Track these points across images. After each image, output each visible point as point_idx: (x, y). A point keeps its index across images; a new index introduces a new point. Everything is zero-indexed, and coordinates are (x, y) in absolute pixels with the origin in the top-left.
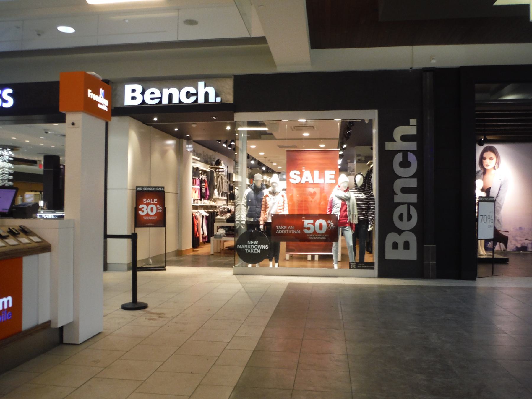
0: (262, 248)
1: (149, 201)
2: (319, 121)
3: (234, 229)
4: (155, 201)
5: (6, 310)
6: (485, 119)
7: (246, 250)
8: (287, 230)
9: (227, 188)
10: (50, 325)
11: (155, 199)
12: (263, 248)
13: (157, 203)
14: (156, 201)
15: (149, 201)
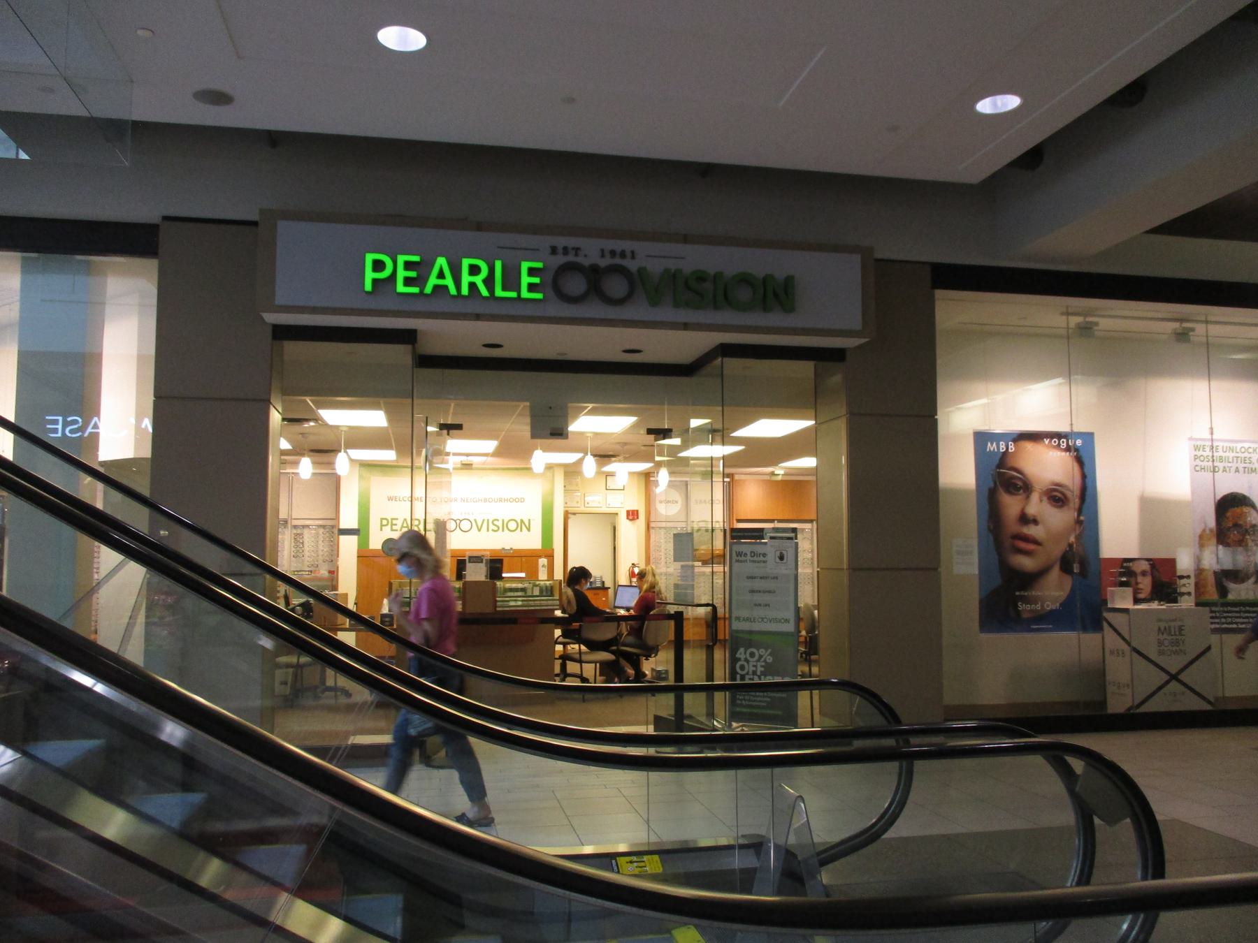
1: (441, 275)
2: (813, 578)
3: (96, 431)
4: (526, 280)
8: (60, 427)
13: (539, 296)
14: (536, 280)
15: (441, 275)
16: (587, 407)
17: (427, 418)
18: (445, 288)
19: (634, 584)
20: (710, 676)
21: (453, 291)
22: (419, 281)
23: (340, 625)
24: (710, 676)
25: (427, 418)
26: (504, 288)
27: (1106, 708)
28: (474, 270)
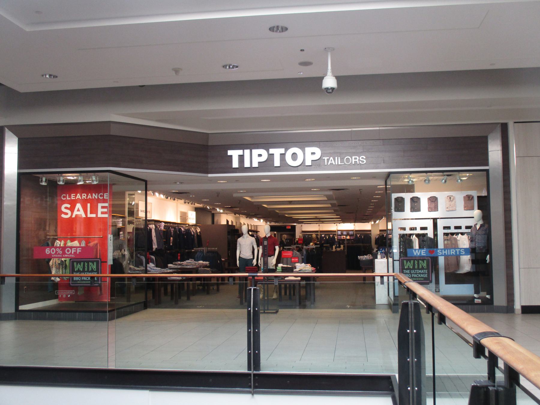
0: (97, 194)
1: (331, 161)
5: (375, 250)
6: (378, 128)
7: (193, 229)
9: (379, 273)
10: (426, 235)
11: (72, 195)
12: (96, 195)
15: (331, 161)
16: (94, 196)
17: (473, 217)
18: (79, 198)
19: (426, 273)
20: (268, 286)
21: (334, 164)
22: (76, 197)
23: (314, 293)
24: (268, 286)
25: (473, 217)
26: (69, 198)
27: (239, 232)
28: (84, 195)
